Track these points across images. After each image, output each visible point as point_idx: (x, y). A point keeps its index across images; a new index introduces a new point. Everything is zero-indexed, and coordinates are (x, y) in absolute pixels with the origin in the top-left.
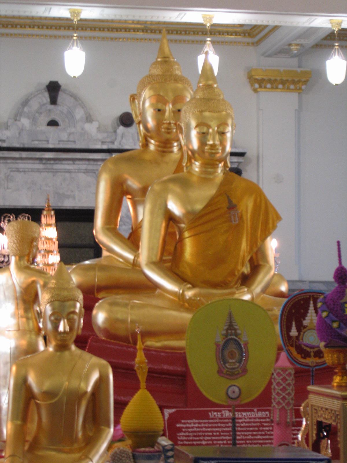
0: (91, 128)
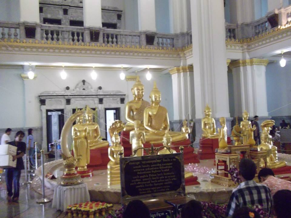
0: (92, 90)
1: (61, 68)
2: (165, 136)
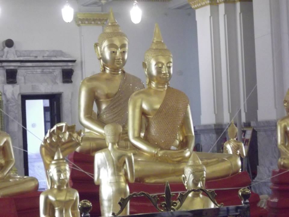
2: (190, 162)
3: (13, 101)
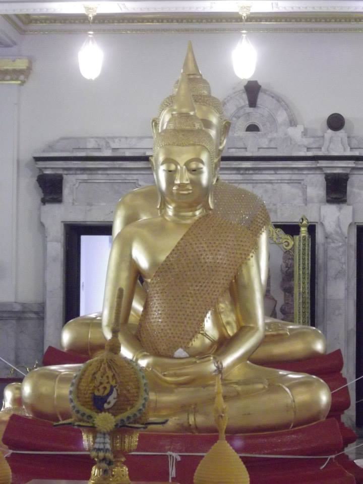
0: (296, 132)
1: (235, 25)
3: (338, 237)
